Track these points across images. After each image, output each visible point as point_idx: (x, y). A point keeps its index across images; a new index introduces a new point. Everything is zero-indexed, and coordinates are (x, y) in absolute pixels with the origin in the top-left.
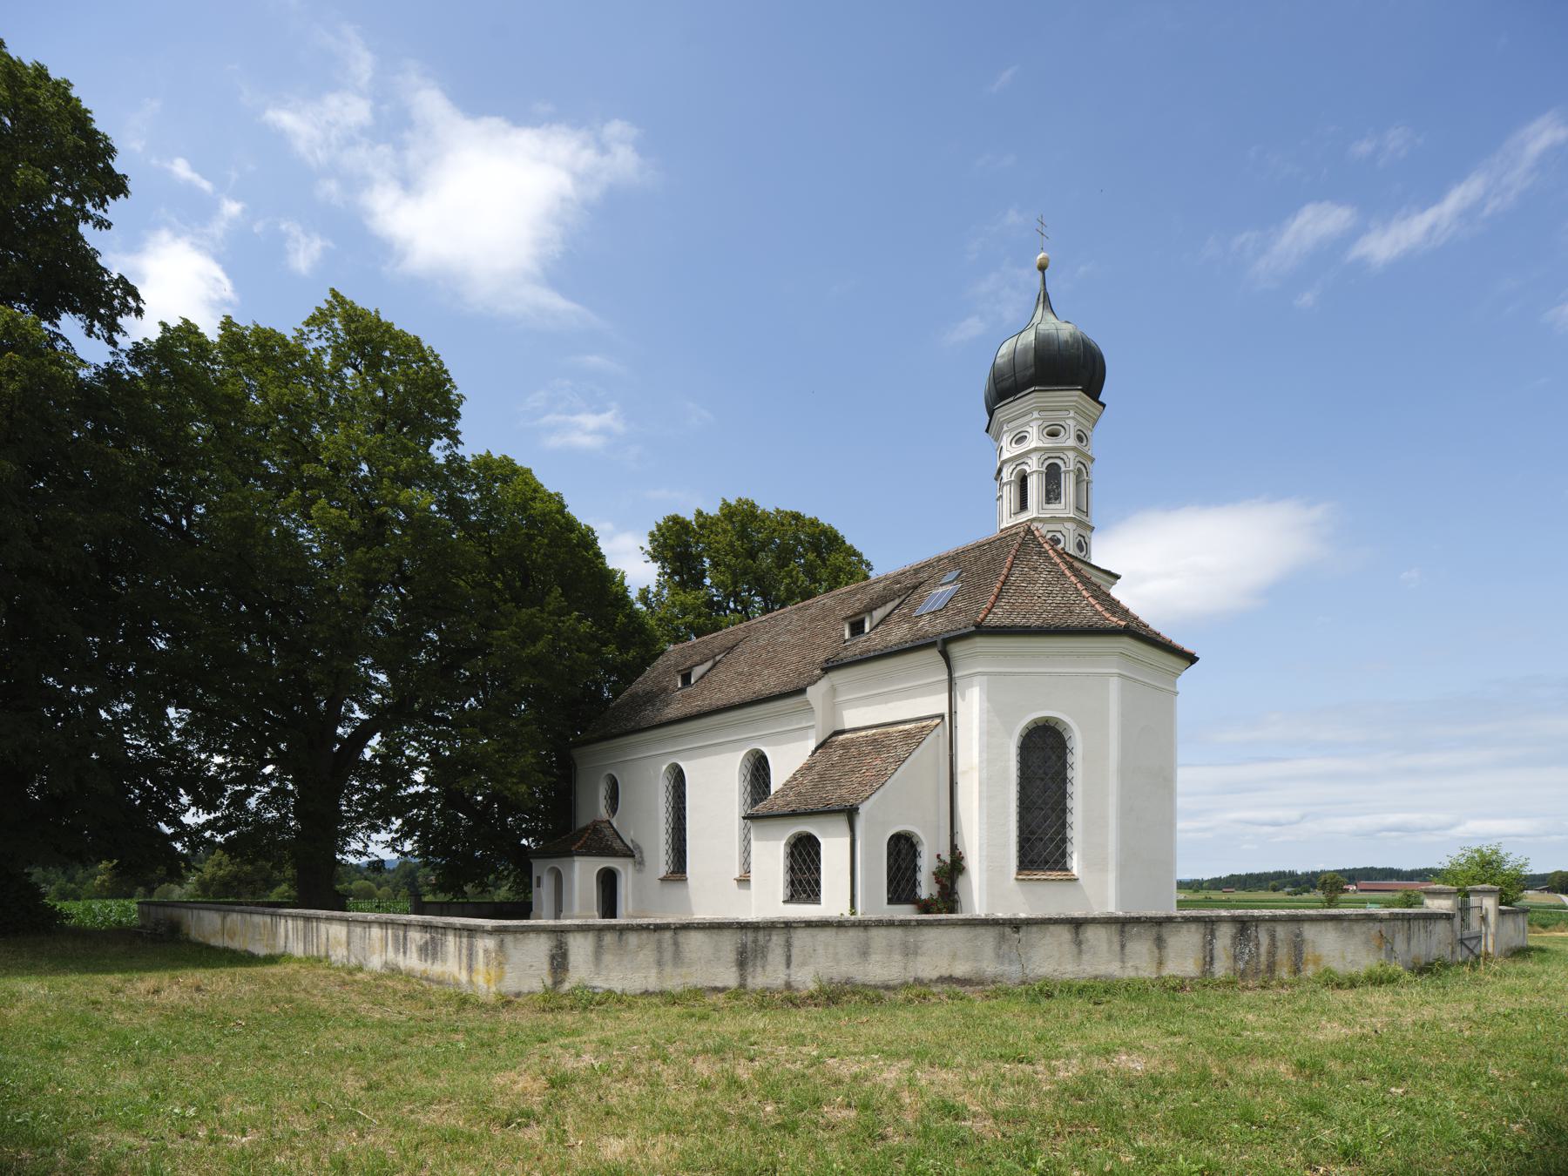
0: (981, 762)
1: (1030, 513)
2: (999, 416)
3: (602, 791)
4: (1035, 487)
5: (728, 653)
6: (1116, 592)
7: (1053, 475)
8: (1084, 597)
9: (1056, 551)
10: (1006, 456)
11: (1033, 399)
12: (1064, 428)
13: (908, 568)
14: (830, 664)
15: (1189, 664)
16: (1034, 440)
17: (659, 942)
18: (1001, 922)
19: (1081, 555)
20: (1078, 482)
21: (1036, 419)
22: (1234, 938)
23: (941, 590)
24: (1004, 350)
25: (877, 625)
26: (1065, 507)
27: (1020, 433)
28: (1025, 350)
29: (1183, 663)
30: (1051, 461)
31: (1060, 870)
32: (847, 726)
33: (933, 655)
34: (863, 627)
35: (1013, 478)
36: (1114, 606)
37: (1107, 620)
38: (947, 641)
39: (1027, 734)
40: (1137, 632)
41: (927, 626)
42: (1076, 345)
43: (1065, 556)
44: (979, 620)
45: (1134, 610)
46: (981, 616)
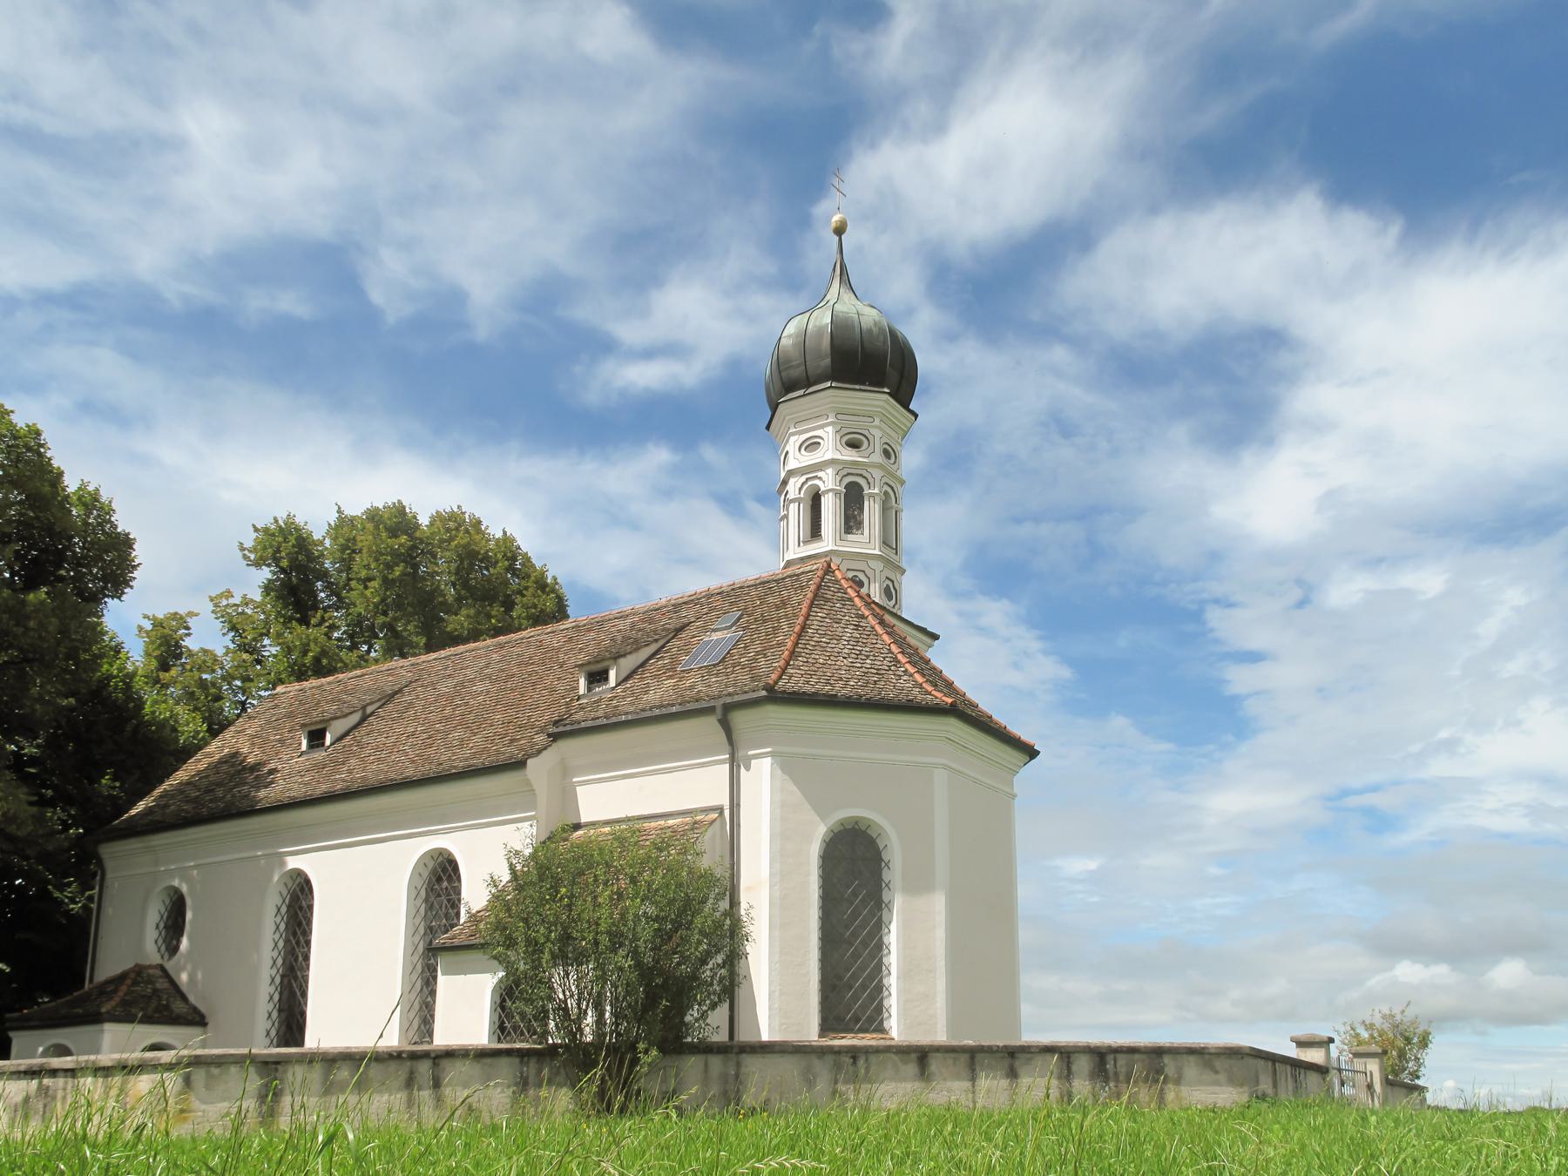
3: (154, 914)
4: (830, 509)
6: (936, 656)
7: (853, 498)
9: (859, 596)
10: (792, 464)
11: (831, 397)
13: (663, 601)
14: (561, 729)
15: (1028, 759)
16: (830, 448)
19: (890, 604)
20: (885, 509)
23: (715, 636)
24: (791, 329)
25: (626, 679)
26: (867, 542)
28: (820, 331)
29: (1021, 757)
31: (875, 1031)
32: (583, 820)
33: (710, 724)
34: (324, 737)
35: (802, 495)
36: (935, 677)
37: (930, 694)
38: (728, 708)
39: (831, 840)
40: (963, 712)
41: (698, 684)
42: (882, 338)
43: (873, 605)
44: (771, 682)
45: (959, 684)
46: (774, 676)
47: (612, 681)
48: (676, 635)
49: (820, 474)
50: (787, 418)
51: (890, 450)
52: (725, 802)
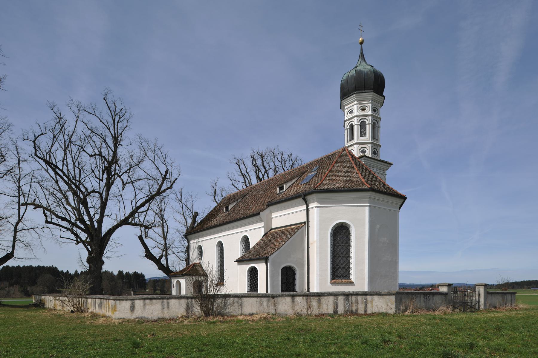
0: (317, 240)
1: (354, 141)
7: (363, 125)
10: (346, 118)
12: (367, 107)
17: (162, 302)
18: (240, 296)
19: (375, 157)
21: (356, 104)
22: (344, 300)
27: (350, 110)
28: (352, 76)
30: (362, 120)
32: (273, 227)
33: (301, 200)
42: (371, 75)
47: (284, 190)
48: (303, 174)
49: (366, 118)
52: (305, 220)
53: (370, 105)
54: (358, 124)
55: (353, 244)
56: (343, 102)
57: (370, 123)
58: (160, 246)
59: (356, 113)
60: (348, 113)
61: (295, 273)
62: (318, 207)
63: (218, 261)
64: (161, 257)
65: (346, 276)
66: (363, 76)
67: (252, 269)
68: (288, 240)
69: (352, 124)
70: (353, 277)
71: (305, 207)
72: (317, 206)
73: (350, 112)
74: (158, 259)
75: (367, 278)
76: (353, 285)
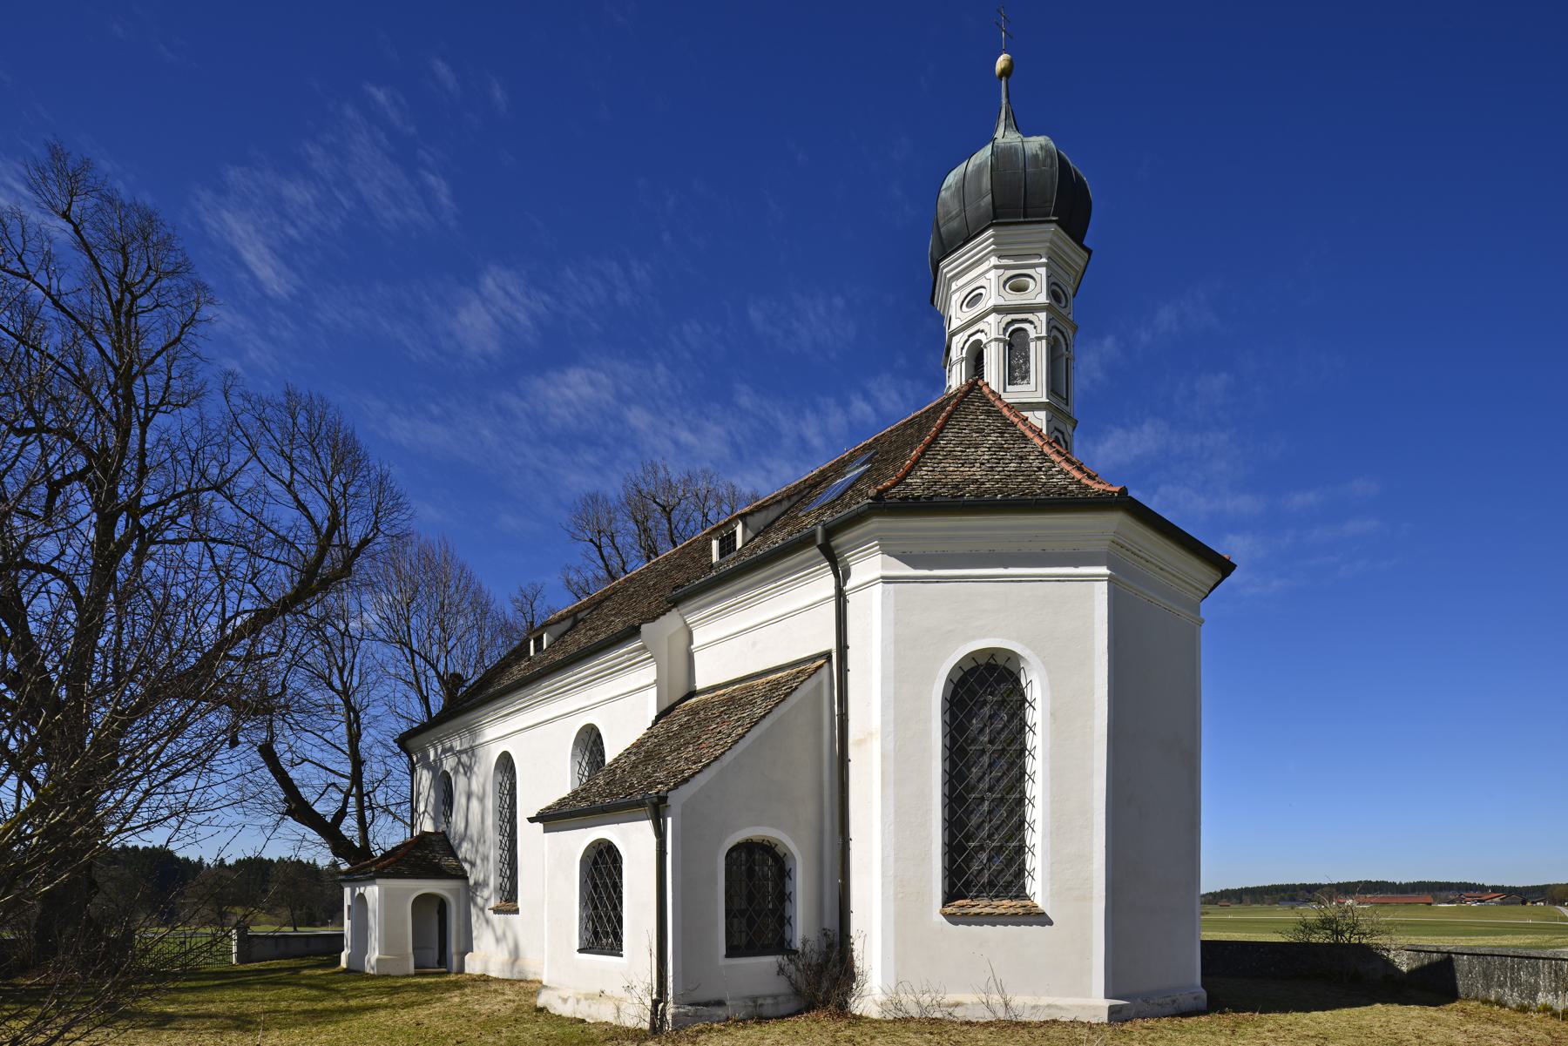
0: (884, 724)
2: (945, 271)
5: (595, 609)
7: (1015, 344)
8: (1053, 462)
12: (1034, 280)
21: (996, 267)
27: (973, 290)
30: (1017, 326)
38: (831, 532)
49: (1030, 316)
50: (948, 276)
51: (1058, 289)
52: (830, 643)
53: (1043, 271)
54: (1002, 337)
55: (1036, 741)
56: (944, 268)
57: (1044, 334)
58: (337, 780)
59: (990, 299)
60: (1004, 286)
61: (787, 869)
62: (887, 580)
63: (501, 823)
64: (341, 815)
65: (1009, 885)
66: (1021, 165)
67: (600, 853)
68: (756, 723)
69: (979, 342)
70: (1037, 889)
71: (825, 584)
72: (882, 577)
73: (974, 297)
74: (329, 821)
75: (1103, 894)
76: (1043, 925)
